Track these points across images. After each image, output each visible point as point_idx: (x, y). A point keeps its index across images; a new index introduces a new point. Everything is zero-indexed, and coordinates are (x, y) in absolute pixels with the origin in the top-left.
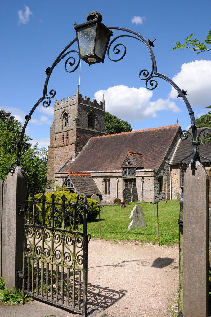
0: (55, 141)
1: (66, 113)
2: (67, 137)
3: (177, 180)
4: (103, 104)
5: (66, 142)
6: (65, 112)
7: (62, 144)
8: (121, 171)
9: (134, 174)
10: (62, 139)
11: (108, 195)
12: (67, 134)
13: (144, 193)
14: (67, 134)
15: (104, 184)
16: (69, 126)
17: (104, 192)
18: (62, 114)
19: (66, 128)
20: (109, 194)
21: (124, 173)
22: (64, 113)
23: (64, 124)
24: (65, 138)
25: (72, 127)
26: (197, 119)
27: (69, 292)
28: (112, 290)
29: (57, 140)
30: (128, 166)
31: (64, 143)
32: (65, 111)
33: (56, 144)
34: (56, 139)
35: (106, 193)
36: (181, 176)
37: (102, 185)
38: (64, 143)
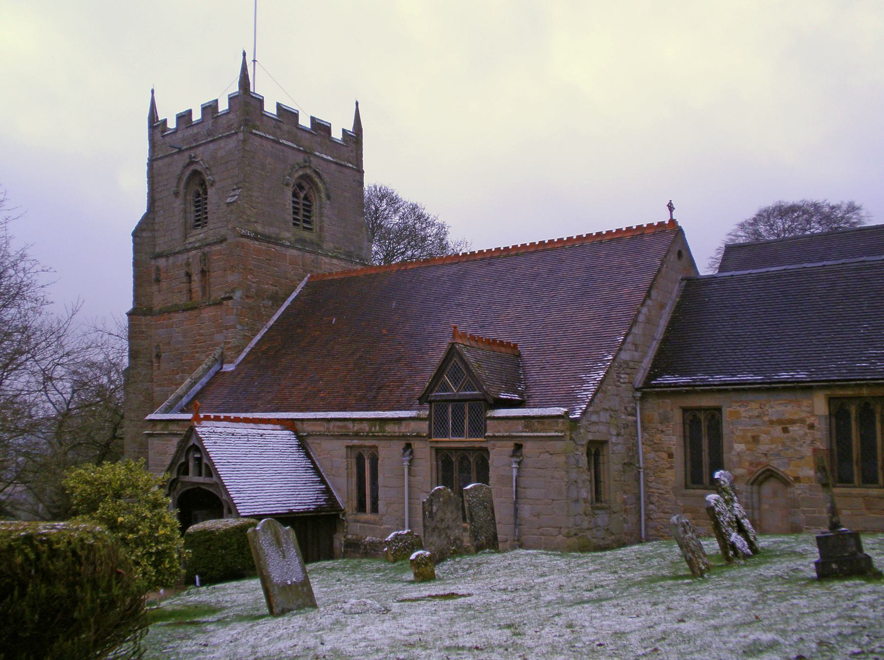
0: (155, 288)
1: (196, 173)
2: (203, 272)
3: (671, 456)
4: (355, 138)
5: (200, 294)
6: (192, 168)
7: (181, 299)
8: (425, 413)
9: (478, 428)
10: (185, 279)
11: (368, 516)
12: (205, 258)
13: (526, 511)
14: (205, 258)
15: (355, 470)
16: (210, 225)
17: (355, 503)
18: (183, 173)
19: (199, 235)
20: (375, 510)
21: (438, 426)
22: (188, 173)
23: (192, 218)
24: (196, 278)
25: (223, 231)
26: (732, 254)
27: (647, 505)
28: (436, 595)
29: (164, 285)
30: (454, 391)
31: (191, 299)
32: (191, 163)
33: (158, 302)
34: (158, 281)
35: (361, 507)
36: (688, 440)
37: (344, 472)
38: (191, 299)
